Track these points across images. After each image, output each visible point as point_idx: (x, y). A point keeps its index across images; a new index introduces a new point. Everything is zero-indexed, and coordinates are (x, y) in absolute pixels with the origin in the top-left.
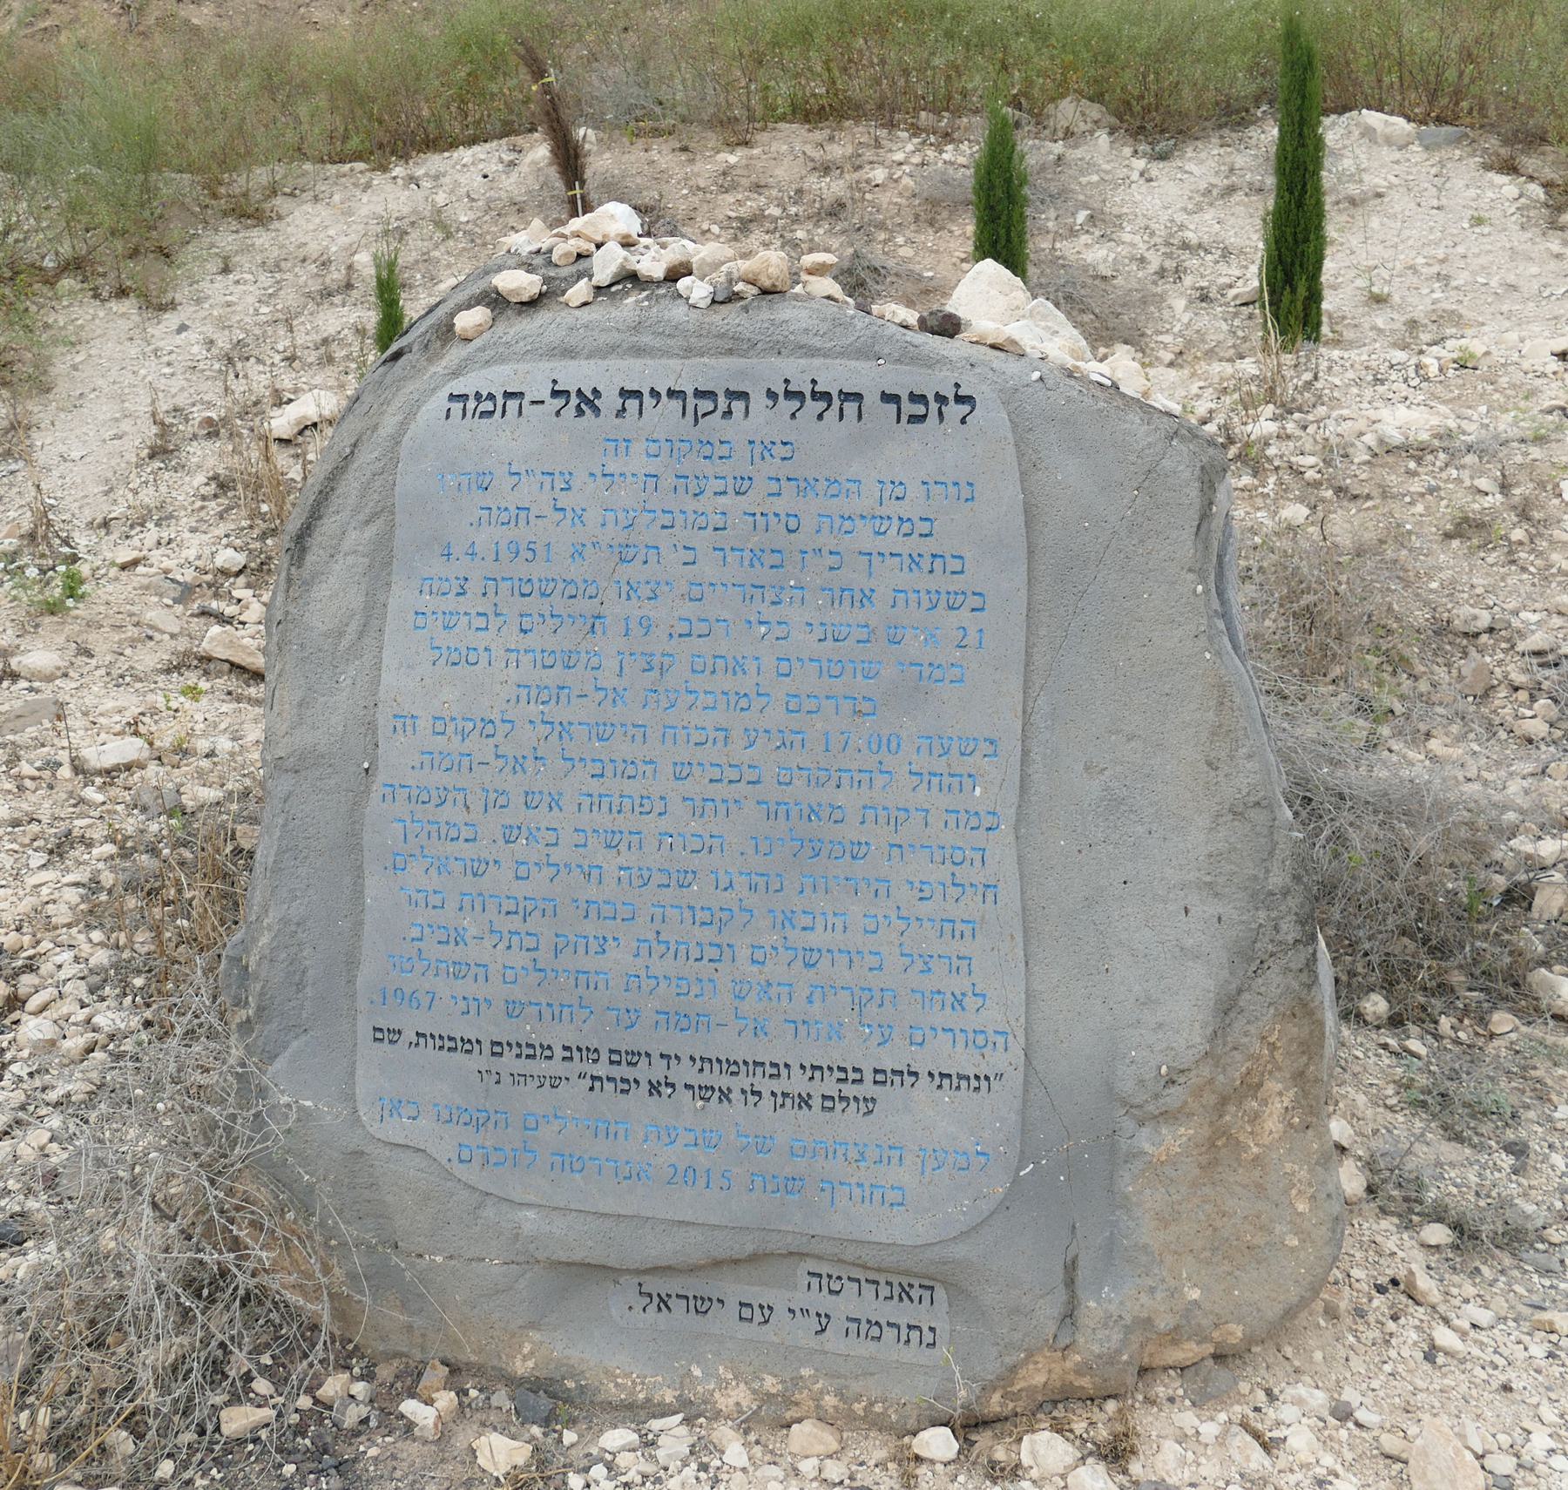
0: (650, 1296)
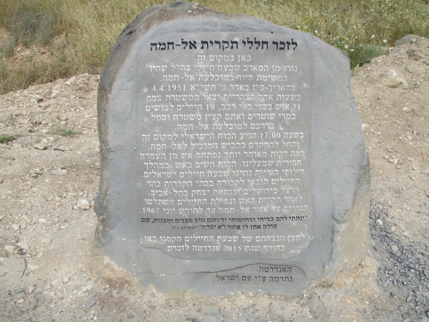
0: (219, 277)
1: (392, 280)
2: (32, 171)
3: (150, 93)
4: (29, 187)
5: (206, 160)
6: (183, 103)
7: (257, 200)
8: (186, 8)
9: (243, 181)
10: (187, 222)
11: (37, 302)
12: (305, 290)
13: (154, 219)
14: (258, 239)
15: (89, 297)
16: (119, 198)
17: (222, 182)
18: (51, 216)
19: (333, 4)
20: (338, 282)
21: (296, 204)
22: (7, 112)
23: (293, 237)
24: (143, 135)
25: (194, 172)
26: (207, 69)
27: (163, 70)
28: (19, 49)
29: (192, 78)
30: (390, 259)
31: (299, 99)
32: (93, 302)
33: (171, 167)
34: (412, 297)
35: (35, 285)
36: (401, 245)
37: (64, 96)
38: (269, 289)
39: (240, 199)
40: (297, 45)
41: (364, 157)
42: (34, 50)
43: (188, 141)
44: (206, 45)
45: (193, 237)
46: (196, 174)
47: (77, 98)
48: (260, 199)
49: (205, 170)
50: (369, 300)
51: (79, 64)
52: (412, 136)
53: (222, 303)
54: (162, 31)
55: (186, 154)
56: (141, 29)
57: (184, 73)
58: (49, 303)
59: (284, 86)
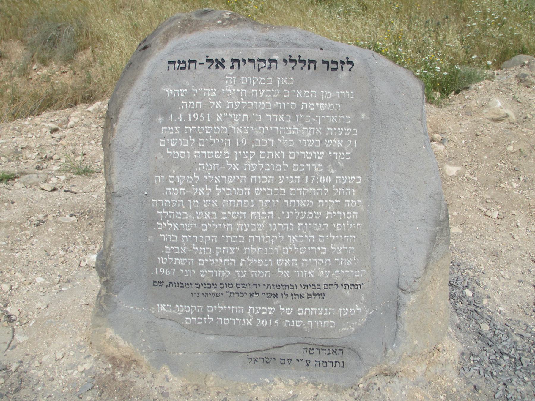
0: (251, 359)
1: (478, 369)
2: (33, 218)
3: (166, 123)
4: (28, 237)
5: (235, 209)
6: (207, 136)
7: (299, 261)
8: (215, 18)
9: (283, 237)
10: (211, 287)
11: (20, 383)
12: (362, 379)
13: (169, 282)
14: (300, 311)
15: (86, 379)
16: (126, 255)
17: (255, 238)
18: (52, 275)
19: (425, 15)
20: (405, 369)
21: (350, 268)
22: (12, 144)
23: (346, 311)
24: (156, 177)
25: (220, 225)
26: (238, 94)
27: (182, 95)
28: (35, 67)
29: (218, 105)
30: (478, 342)
31: (356, 134)
32: (91, 386)
33: (190, 217)
34: (503, 392)
35: (21, 362)
36: (493, 323)
37: (84, 126)
38: (315, 377)
39: (277, 260)
40: (353, 66)
41: (441, 209)
42: (53, 68)
43: (212, 184)
44: (237, 64)
45: (217, 307)
46: (223, 226)
47: (100, 128)
48: (303, 260)
49: (234, 222)
50: (445, 395)
51: (106, 86)
52: (517, 184)
53: (253, 393)
54: (183, 46)
55: (210, 201)
56: (157, 43)
57: (208, 98)
58: (35, 385)
59: (336, 117)
